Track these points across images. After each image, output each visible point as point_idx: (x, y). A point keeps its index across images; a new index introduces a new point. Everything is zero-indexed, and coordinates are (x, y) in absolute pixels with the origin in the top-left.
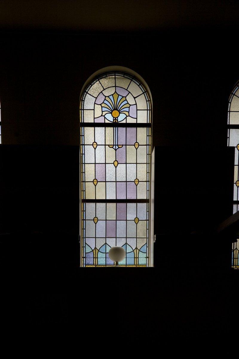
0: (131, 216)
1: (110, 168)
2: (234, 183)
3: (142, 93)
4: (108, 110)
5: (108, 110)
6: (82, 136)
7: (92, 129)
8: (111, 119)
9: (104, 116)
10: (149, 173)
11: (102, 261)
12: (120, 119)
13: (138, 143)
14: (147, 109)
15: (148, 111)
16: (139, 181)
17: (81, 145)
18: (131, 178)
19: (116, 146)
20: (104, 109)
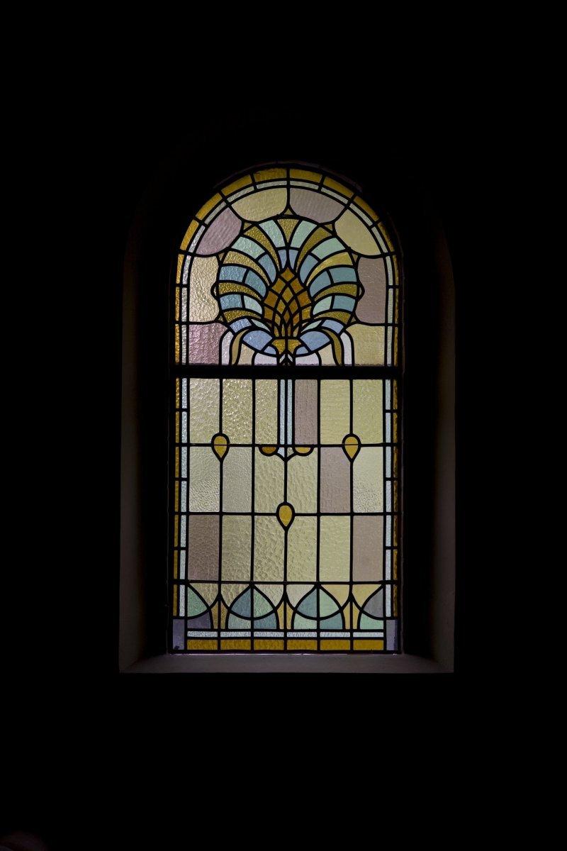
6: (181, 286)
13: (356, 437)
15: (390, 328)
16: (360, 445)
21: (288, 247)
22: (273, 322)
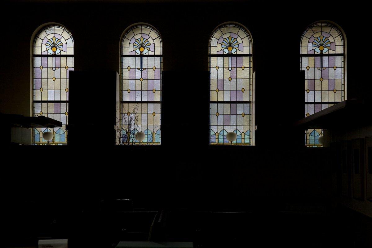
0: (240, 112)
1: (227, 82)
2: (305, 91)
4: (137, 47)
5: (137, 47)
7: (215, 58)
8: (139, 53)
9: (223, 50)
10: (251, 84)
11: (221, 140)
12: (144, 53)
17: (162, 68)
18: (240, 88)
19: (230, 68)
20: (223, 46)
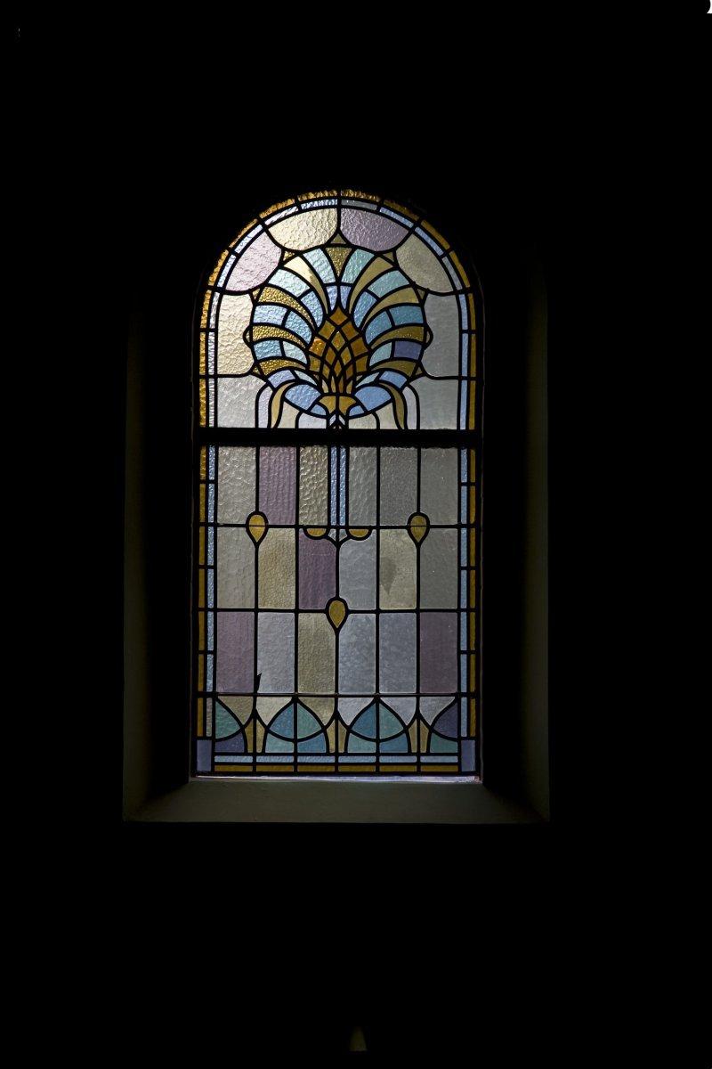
3: (454, 521)
6: (207, 482)
14: (457, 374)
21: (338, 283)
22: (320, 374)
